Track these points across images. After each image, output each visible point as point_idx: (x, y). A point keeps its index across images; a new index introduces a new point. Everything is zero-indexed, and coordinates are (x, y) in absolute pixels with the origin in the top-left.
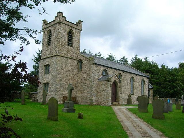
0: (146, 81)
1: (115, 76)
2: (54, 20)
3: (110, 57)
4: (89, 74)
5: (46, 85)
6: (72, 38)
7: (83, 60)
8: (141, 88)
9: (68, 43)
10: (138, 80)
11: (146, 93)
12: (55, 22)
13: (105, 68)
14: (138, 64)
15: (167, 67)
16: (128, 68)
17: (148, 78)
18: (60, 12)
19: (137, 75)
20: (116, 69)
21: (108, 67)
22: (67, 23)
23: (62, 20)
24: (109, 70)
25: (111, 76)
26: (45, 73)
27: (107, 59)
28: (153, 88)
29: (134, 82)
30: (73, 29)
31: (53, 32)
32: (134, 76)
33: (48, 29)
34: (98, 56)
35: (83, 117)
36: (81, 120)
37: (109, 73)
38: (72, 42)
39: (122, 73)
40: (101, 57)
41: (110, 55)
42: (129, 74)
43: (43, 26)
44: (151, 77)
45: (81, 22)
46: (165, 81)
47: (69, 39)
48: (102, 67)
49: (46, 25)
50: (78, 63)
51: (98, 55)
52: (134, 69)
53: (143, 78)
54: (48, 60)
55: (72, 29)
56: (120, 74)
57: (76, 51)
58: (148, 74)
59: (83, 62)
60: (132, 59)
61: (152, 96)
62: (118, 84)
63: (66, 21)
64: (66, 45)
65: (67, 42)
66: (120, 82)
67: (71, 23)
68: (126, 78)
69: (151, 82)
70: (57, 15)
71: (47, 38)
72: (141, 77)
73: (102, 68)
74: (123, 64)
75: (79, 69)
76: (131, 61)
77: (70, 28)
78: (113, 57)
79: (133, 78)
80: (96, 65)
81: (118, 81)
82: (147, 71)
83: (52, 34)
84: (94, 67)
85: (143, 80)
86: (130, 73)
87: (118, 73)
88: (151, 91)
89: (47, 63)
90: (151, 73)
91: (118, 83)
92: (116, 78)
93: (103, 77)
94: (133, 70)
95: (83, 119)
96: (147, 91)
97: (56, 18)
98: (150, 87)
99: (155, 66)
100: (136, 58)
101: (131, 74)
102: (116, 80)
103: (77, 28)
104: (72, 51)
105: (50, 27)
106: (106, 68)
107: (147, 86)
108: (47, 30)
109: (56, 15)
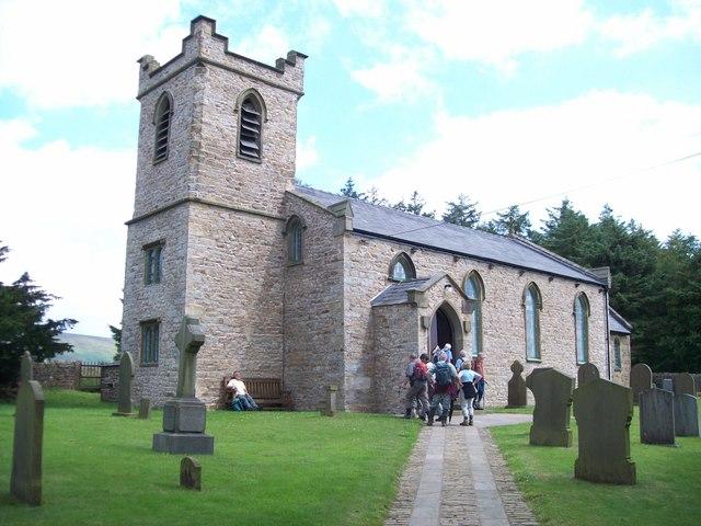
0: (598, 301)
1: (445, 282)
2: (180, 52)
3: (458, 210)
4: (333, 276)
5: (149, 329)
6: (259, 127)
7: (307, 216)
8: (581, 336)
9: (242, 147)
10: (560, 296)
11: (599, 355)
12: (183, 62)
13: (407, 249)
14: (573, 240)
15: (632, 224)
16: (518, 248)
17: (604, 289)
18: (201, 18)
19: (552, 276)
20: (457, 255)
21: (416, 246)
22: (235, 64)
23: (211, 50)
24: (418, 258)
25: (427, 284)
26: (148, 282)
27: (447, 219)
28: (633, 331)
29: (541, 308)
30: (264, 91)
31: (176, 105)
32: (542, 282)
33: (160, 91)
34: (411, 209)
35: (199, 479)
36: (191, 493)
37: (419, 273)
38: (259, 145)
39: (482, 269)
40: (422, 213)
41: (457, 203)
42: (516, 273)
43: (142, 79)
44: (623, 288)
45: (299, 60)
46: (683, 302)
47: (243, 130)
48: (387, 247)
49: (151, 76)
50: (284, 234)
51: (410, 206)
52: (559, 262)
53: (583, 288)
54: (158, 223)
55: (260, 90)
56: (475, 277)
57: (278, 179)
58: (605, 273)
59: (305, 228)
60: (549, 219)
61: (629, 366)
62: (462, 317)
63: (227, 53)
64: (233, 156)
65: (234, 143)
66: (472, 305)
67: (254, 62)
68: (503, 290)
69: (618, 307)
70: (192, 29)
71: (154, 129)
72: (572, 285)
73: (389, 252)
74: (510, 236)
75: (290, 259)
76: (546, 227)
77: (253, 85)
78: (471, 212)
79: (534, 290)
80: (360, 239)
81: (457, 303)
82: (596, 263)
83: (172, 114)
84: (350, 247)
85: (584, 299)
86: (522, 270)
87: (463, 268)
88: (625, 347)
89: (155, 237)
90: (616, 265)
91: (459, 312)
92: (450, 289)
93: (392, 292)
94: (539, 257)
95: (199, 489)
96: (604, 346)
97: (189, 44)
98: (615, 326)
99: (639, 241)
100: (564, 210)
101: (526, 274)
102: (451, 301)
103: (282, 84)
104: (258, 183)
105: (166, 85)
106: (408, 251)
107: (602, 323)
108: (154, 97)
109: (188, 33)
